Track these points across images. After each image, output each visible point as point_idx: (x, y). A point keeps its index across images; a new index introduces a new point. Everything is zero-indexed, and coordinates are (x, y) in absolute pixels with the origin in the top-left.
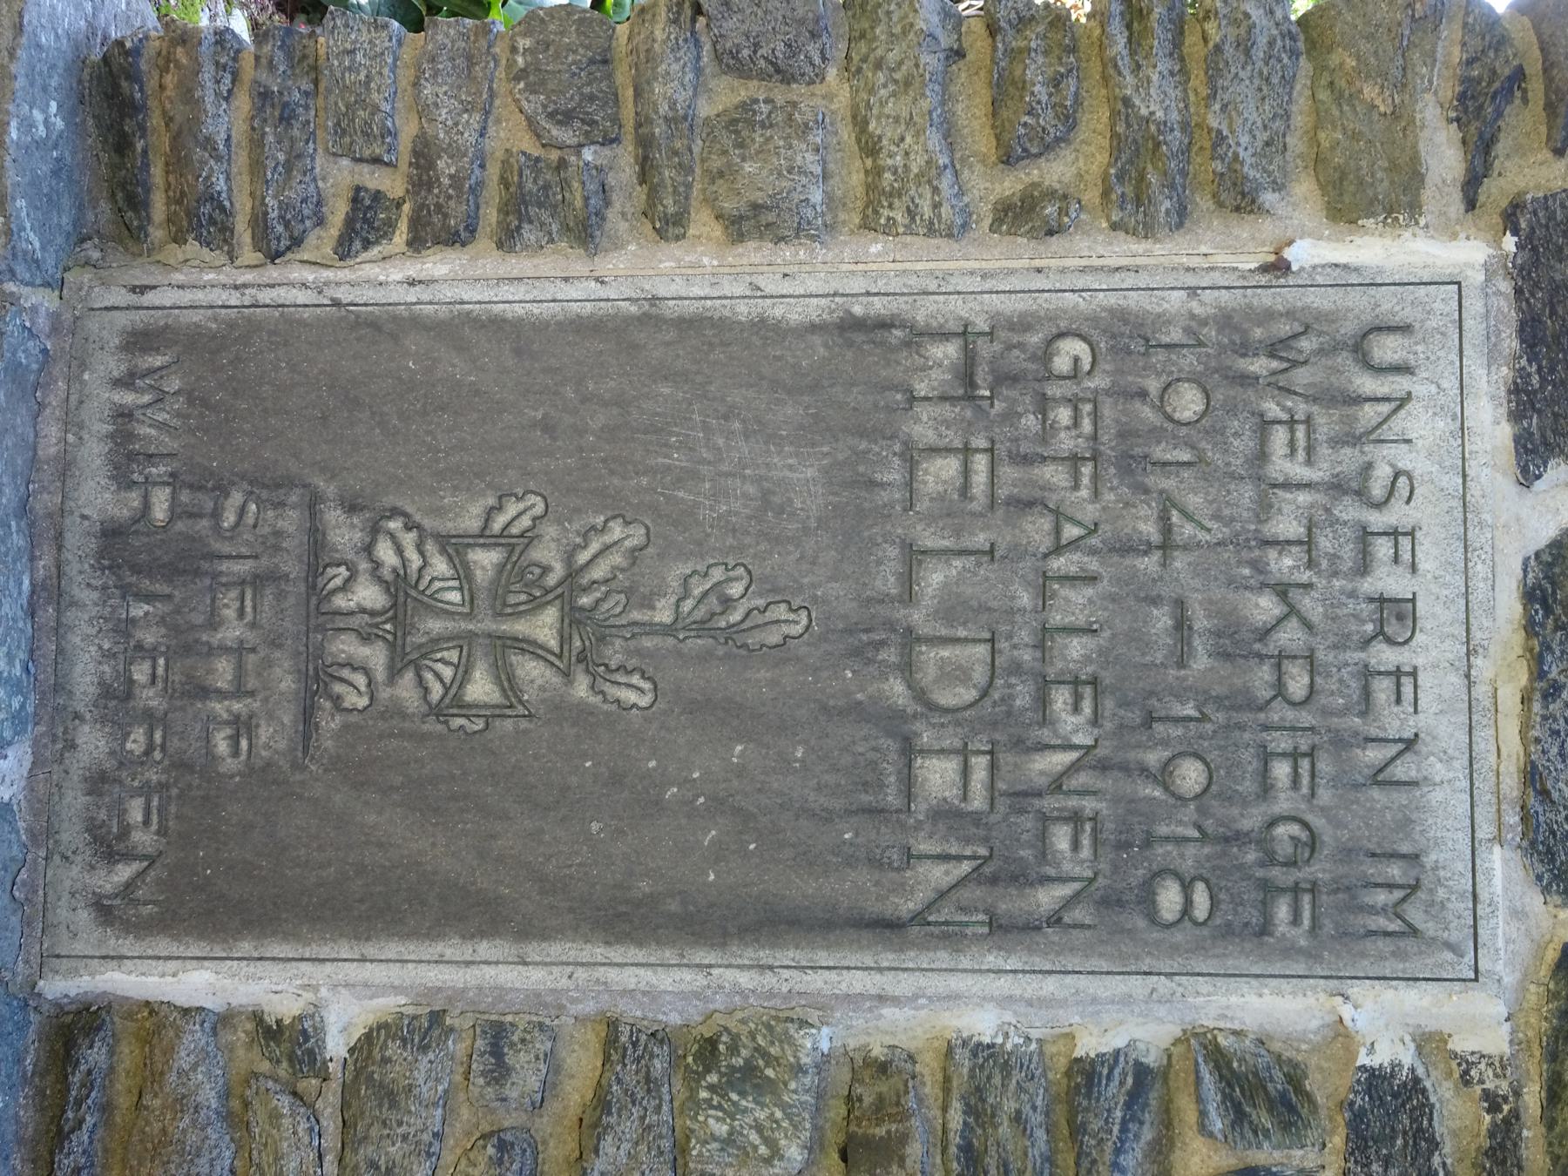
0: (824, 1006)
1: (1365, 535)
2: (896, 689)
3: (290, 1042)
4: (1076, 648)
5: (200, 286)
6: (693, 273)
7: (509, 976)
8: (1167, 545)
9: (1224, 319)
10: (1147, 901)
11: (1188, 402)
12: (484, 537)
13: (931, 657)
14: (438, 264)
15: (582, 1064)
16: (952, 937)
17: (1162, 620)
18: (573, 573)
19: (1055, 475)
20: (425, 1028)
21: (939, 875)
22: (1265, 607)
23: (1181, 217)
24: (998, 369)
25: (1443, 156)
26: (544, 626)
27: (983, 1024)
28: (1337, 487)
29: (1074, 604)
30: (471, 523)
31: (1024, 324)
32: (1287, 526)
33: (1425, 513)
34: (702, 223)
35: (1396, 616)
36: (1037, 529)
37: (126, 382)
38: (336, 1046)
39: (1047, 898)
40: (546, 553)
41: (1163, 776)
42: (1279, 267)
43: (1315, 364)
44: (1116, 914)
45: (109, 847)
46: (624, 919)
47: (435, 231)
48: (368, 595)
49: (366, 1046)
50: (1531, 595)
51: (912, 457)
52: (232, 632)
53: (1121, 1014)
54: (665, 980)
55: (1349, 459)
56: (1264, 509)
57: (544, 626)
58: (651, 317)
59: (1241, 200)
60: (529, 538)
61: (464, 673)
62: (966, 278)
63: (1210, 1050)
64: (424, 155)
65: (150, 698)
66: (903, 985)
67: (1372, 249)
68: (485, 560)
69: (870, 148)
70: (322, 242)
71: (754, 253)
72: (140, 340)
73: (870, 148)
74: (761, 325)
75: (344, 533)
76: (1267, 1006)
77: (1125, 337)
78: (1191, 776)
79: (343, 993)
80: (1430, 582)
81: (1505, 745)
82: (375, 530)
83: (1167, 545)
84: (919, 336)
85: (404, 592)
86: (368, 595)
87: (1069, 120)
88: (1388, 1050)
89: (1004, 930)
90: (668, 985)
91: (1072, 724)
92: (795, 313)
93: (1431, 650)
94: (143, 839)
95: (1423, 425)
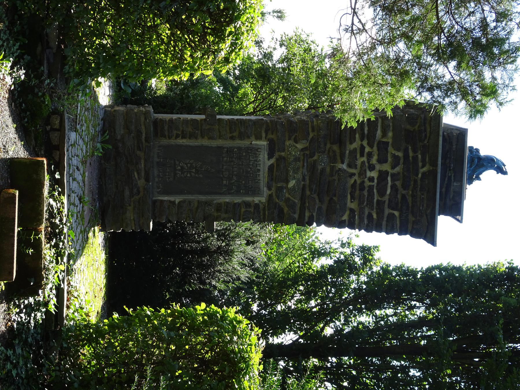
0: (215, 199)
1: (257, 164)
2: (222, 176)
3: (173, 203)
4: (235, 172)
5: (165, 142)
6: (205, 142)
7: (191, 197)
8: (242, 165)
9: (247, 147)
10: (240, 192)
11: (244, 154)
12: (189, 163)
13: (224, 173)
14: (184, 141)
15: (196, 204)
16: (226, 194)
17: (242, 170)
18: (196, 166)
19: (234, 159)
20: (184, 201)
21: (224, 190)
22: (249, 169)
23: (244, 139)
24: (230, 150)
25: (264, 135)
26: (194, 170)
27: (227, 200)
28: (255, 161)
29: (235, 169)
30: (188, 162)
31: (232, 147)
32: (251, 164)
33: (261, 163)
34: (206, 137)
35: (259, 170)
36: (232, 163)
37: (158, 150)
38: (177, 203)
39: (233, 191)
40: (194, 165)
41: (241, 182)
42: (251, 144)
43: (255, 151)
44: (238, 193)
45: (158, 188)
46: (201, 193)
47: (183, 137)
48: (179, 168)
49: (179, 203)
50: (269, 169)
51: (223, 158)
52: (168, 171)
53: (238, 200)
54: (203, 198)
55: (256, 159)
56: (250, 162)
57: (194, 170)
58: (202, 146)
59: (249, 137)
60: (192, 163)
61: (187, 174)
62: (228, 143)
63: (244, 202)
64: (183, 131)
65: (161, 176)
66: (222, 198)
67: (258, 142)
68: (189, 165)
69: (220, 132)
70: (174, 137)
71: (211, 141)
72: (160, 146)
73: (220, 132)
74: (211, 147)
75: (177, 163)
76: (248, 199)
77: (239, 148)
78: (243, 182)
79: (177, 199)
80: (261, 168)
81: (266, 180)
82: (180, 163)
83: (242, 165)
84: (224, 148)
85: (182, 167)
86: (179, 168)
87: (235, 131)
88: (257, 202)
89: (229, 194)
90: (203, 198)
91: (235, 178)
92: (214, 146)
93: (261, 173)
94: (161, 187)
95: (261, 156)
